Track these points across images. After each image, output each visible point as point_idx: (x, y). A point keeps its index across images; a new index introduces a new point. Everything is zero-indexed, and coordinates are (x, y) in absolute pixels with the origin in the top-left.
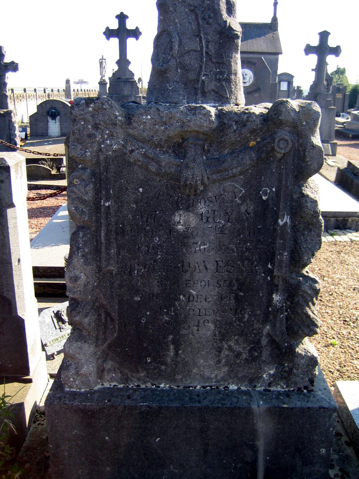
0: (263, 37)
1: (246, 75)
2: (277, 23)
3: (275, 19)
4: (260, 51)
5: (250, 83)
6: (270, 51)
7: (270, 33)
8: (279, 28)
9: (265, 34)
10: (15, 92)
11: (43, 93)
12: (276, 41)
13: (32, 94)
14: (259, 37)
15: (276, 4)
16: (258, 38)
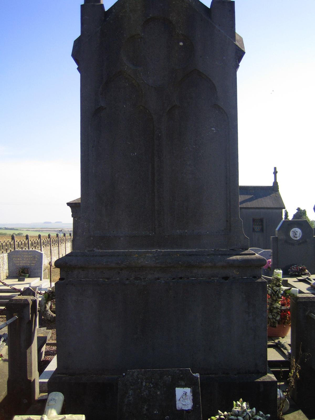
0: (268, 197)
1: (297, 232)
2: (278, 186)
3: (275, 183)
4: (268, 207)
5: (300, 238)
6: (276, 207)
7: (273, 193)
8: (279, 190)
9: (270, 194)
10: (16, 239)
11: (25, 240)
12: (279, 199)
13: (23, 242)
14: (266, 196)
15: (275, 173)
16: (265, 197)
